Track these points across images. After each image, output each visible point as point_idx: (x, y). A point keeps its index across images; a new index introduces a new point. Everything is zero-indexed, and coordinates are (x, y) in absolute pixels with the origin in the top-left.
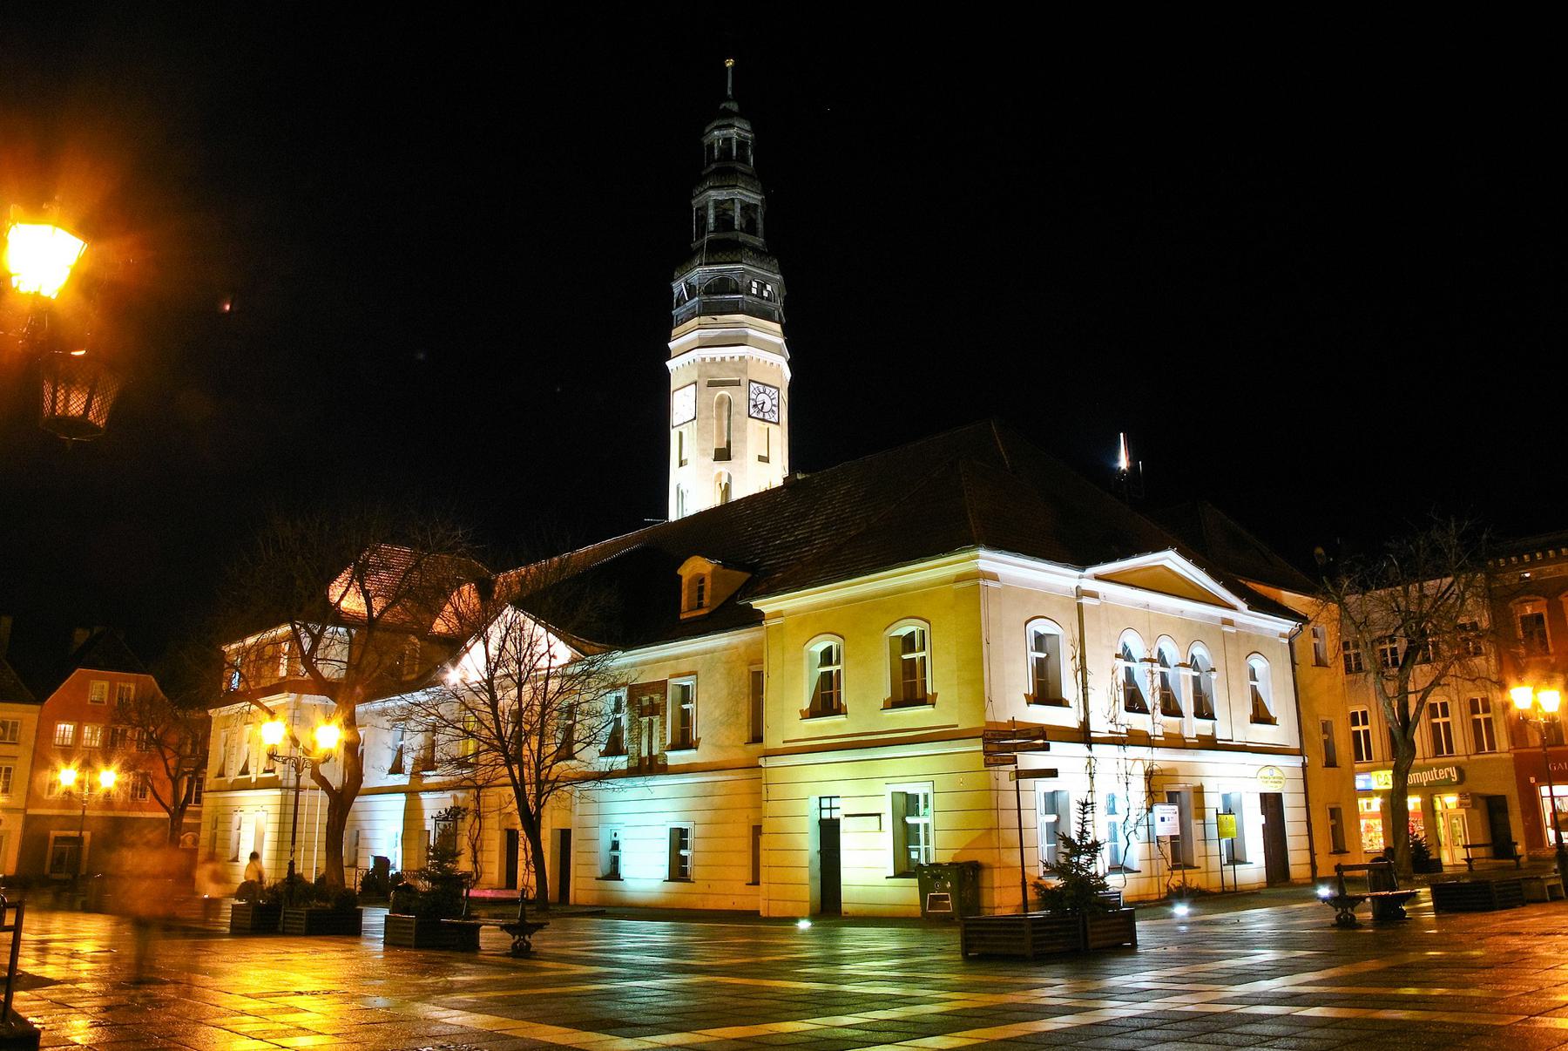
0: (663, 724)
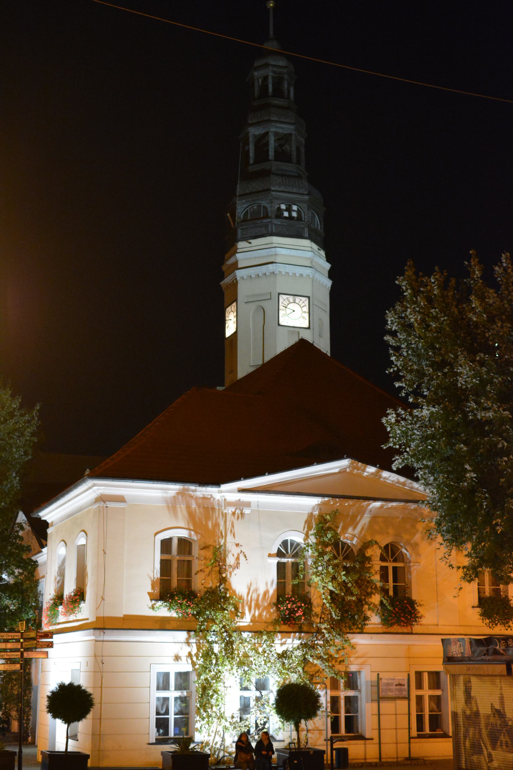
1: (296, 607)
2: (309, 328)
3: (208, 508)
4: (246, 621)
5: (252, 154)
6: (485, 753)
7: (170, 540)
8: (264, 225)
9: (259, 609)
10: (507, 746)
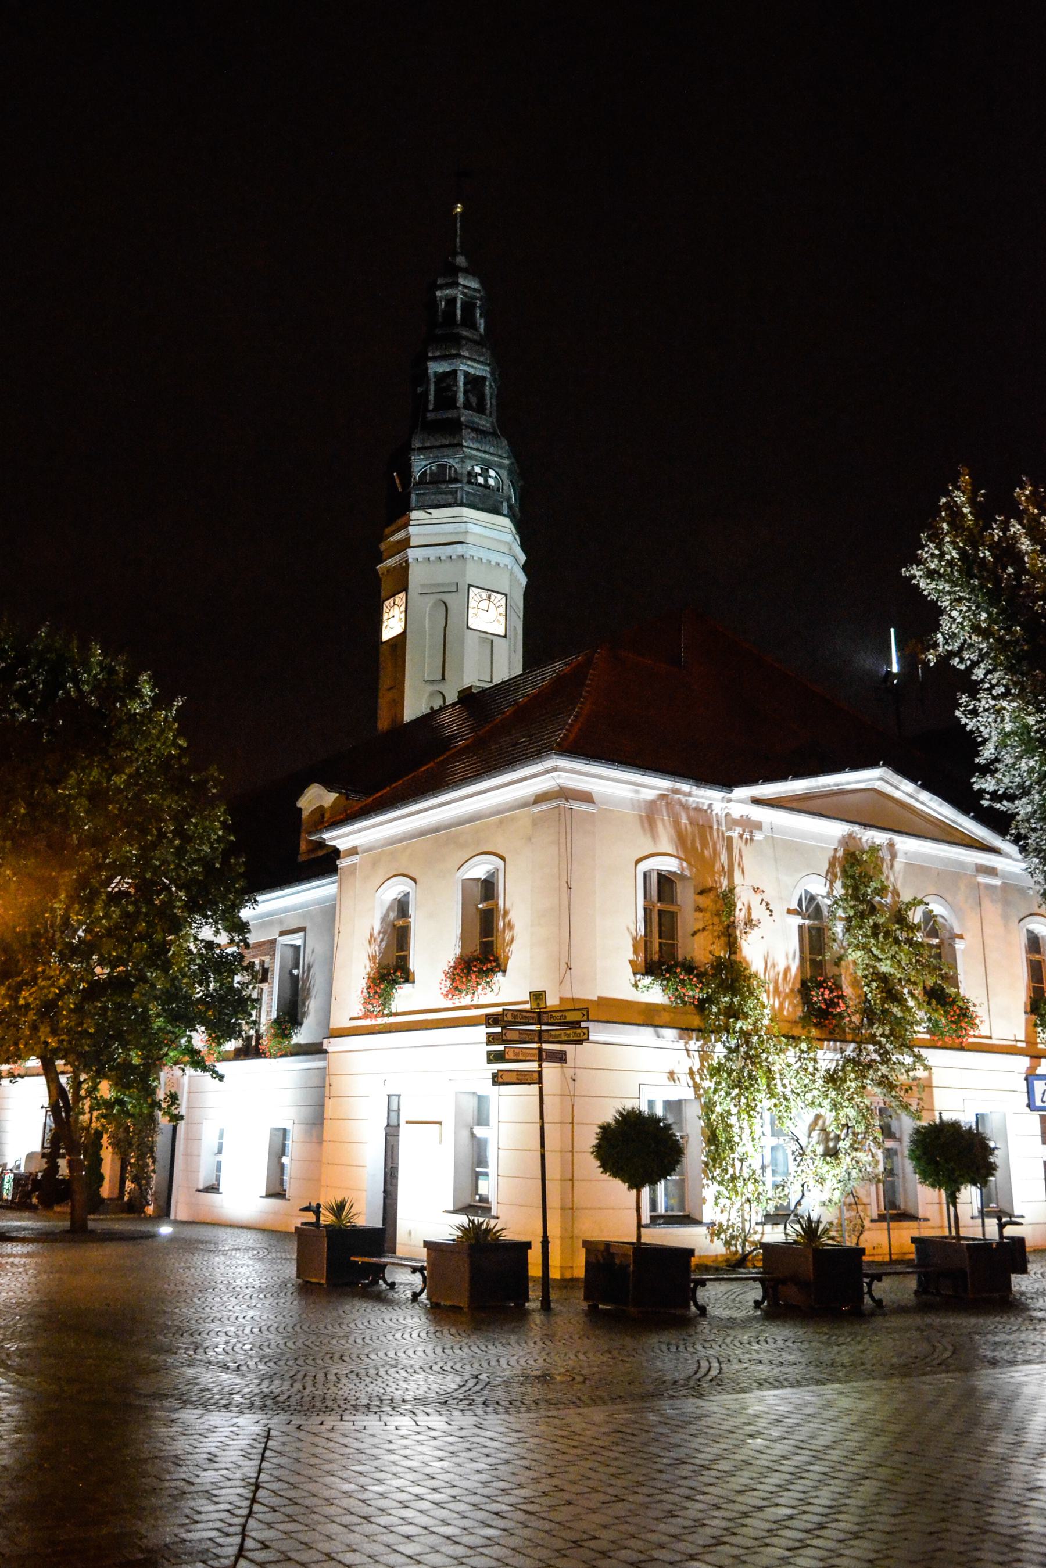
0: (271, 993)
2: (505, 636)
8: (444, 490)
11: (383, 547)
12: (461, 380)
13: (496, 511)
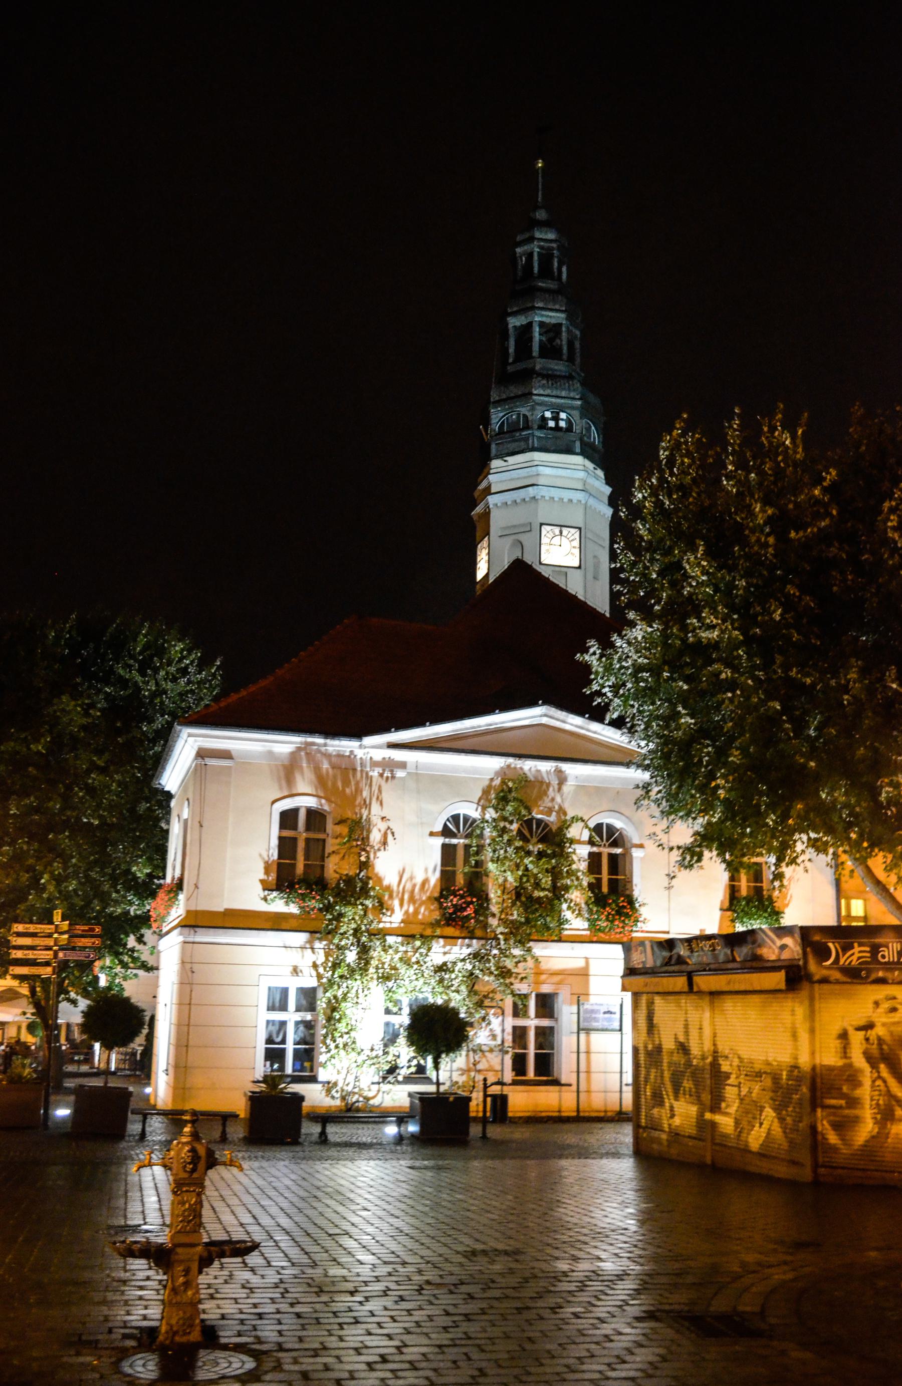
1: (464, 903)
2: (579, 567)
3: (347, 768)
4: (395, 919)
5: (511, 350)
6: (667, 1105)
7: (295, 812)
8: (519, 438)
9: (414, 903)
10: (691, 1095)
11: (476, 494)
12: (536, 329)
13: (569, 451)
